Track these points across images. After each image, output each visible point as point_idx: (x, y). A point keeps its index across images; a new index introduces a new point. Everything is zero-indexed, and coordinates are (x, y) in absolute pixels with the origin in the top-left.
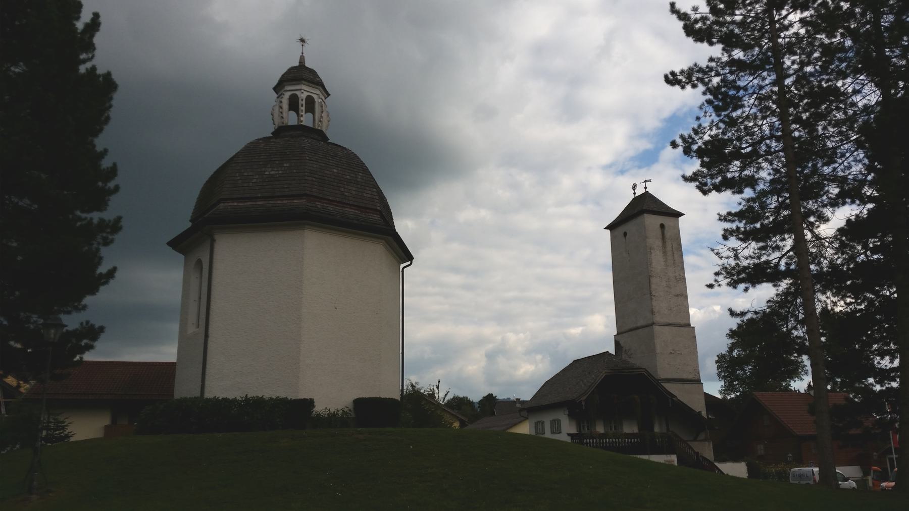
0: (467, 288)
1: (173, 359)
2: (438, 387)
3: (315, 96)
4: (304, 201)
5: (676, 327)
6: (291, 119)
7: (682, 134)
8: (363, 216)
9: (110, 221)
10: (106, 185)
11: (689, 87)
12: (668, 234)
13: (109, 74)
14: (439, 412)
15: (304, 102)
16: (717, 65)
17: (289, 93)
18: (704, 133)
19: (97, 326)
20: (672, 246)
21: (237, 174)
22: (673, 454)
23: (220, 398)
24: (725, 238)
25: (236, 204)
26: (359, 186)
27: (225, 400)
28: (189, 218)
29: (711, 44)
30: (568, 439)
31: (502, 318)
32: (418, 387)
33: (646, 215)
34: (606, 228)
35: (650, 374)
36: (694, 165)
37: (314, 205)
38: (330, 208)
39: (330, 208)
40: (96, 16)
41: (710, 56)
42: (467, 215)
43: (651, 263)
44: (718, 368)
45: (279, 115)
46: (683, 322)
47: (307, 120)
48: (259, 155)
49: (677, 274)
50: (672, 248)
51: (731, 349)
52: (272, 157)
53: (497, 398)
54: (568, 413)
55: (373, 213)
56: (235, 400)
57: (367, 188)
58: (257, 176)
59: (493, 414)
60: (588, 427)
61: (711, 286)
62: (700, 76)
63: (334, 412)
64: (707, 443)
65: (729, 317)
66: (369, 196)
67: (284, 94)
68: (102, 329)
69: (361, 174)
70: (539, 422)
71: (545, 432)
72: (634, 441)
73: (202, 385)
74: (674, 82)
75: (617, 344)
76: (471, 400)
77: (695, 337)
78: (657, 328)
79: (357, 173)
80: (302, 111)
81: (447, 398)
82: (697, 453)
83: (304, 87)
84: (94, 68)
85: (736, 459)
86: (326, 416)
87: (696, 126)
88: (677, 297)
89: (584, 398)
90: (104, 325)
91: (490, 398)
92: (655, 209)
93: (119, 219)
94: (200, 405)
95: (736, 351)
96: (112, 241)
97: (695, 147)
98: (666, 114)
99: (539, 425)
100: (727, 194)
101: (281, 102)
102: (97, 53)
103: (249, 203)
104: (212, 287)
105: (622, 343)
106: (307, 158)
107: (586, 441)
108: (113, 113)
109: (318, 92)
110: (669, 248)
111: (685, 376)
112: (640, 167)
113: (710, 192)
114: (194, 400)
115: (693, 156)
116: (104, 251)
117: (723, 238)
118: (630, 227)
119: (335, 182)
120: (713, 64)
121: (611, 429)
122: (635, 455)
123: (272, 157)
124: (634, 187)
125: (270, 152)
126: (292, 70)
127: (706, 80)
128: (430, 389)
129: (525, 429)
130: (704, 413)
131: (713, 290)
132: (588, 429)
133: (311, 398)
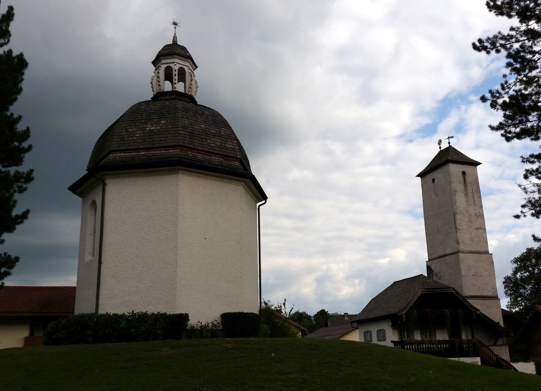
0: (297, 229)
1: (74, 285)
2: (284, 304)
3: (185, 68)
4: (178, 150)
5: (477, 255)
6: (167, 86)
7: (491, 90)
8: (227, 163)
9: (24, 173)
10: (21, 145)
11: (493, 52)
12: (469, 179)
13: (22, 55)
14: (286, 324)
15: (177, 73)
16: (517, 34)
17: (165, 66)
18: (509, 88)
19: (13, 257)
20: (472, 190)
21: (124, 131)
22: (478, 356)
23: (111, 314)
24: (526, 177)
25: (122, 154)
26: (223, 139)
27: (115, 315)
28: (86, 168)
29: (510, 16)
30: (392, 345)
31: (326, 252)
32: (270, 304)
33: (450, 164)
34: (417, 176)
35: (458, 292)
36: (498, 117)
37: (186, 154)
38: (200, 156)
39: (200, 156)
40: (11, 9)
41: (511, 26)
42: (295, 174)
43: (456, 203)
44: (505, 287)
45: (157, 84)
46: (483, 250)
47: (180, 87)
48: (141, 115)
49: (476, 212)
50: (472, 191)
51: (515, 273)
52: (152, 116)
53: (328, 313)
54: (391, 324)
55: (234, 161)
56: (123, 316)
57: (229, 140)
58: (140, 132)
59: (326, 325)
60: (408, 335)
61: (517, 217)
62: (503, 42)
63: (205, 325)
64: (504, 347)
65: (533, 241)
66: (230, 146)
67: (160, 66)
68: (17, 259)
69: (224, 129)
70: (367, 332)
71: (386, 339)
72: (446, 346)
73: (96, 303)
74: (481, 48)
75: (429, 268)
76: (309, 314)
77: (492, 262)
78: (461, 255)
79: (220, 128)
80: (175, 80)
81: (293, 312)
82: (497, 356)
83: (176, 60)
84: (10, 52)
85: (526, 360)
86: (199, 328)
87: (503, 82)
88: (478, 230)
89: (405, 312)
90: (18, 256)
91: (323, 313)
92: (458, 160)
93: (32, 171)
94: (95, 320)
95: (519, 273)
96: (26, 189)
97: (500, 101)
98: (441, 96)
99: (368, 334)
100: (527, 141)
101: (158, 73)
102: (12, 38)
103: (133, 154)
104: (104, 223)
105: (433, 267)
106: (180, 116)
107: (407, 347)
108: (24, 85)
109: (188, 64)
110: (470, 190)
111: (485, 294)
112: (423, 137)
113: (513, 139)
114: (90, 316)
115: (498, 109)
116: (17, 196)
117: (524, 177)
118: (437, 174)
119: (203, 135)
120: (513, 33)
121: (426, 337)
122: (447, 358)
123: (152, 116)
124: (440, 142)
125: (150, 112)
126: (166, 47)
127: (508, 46)
128: (278, 306)
129: (356, 337)
130: (502, 324)
131: (519, 220)
132: (408, 337)
133: (186, 313)
